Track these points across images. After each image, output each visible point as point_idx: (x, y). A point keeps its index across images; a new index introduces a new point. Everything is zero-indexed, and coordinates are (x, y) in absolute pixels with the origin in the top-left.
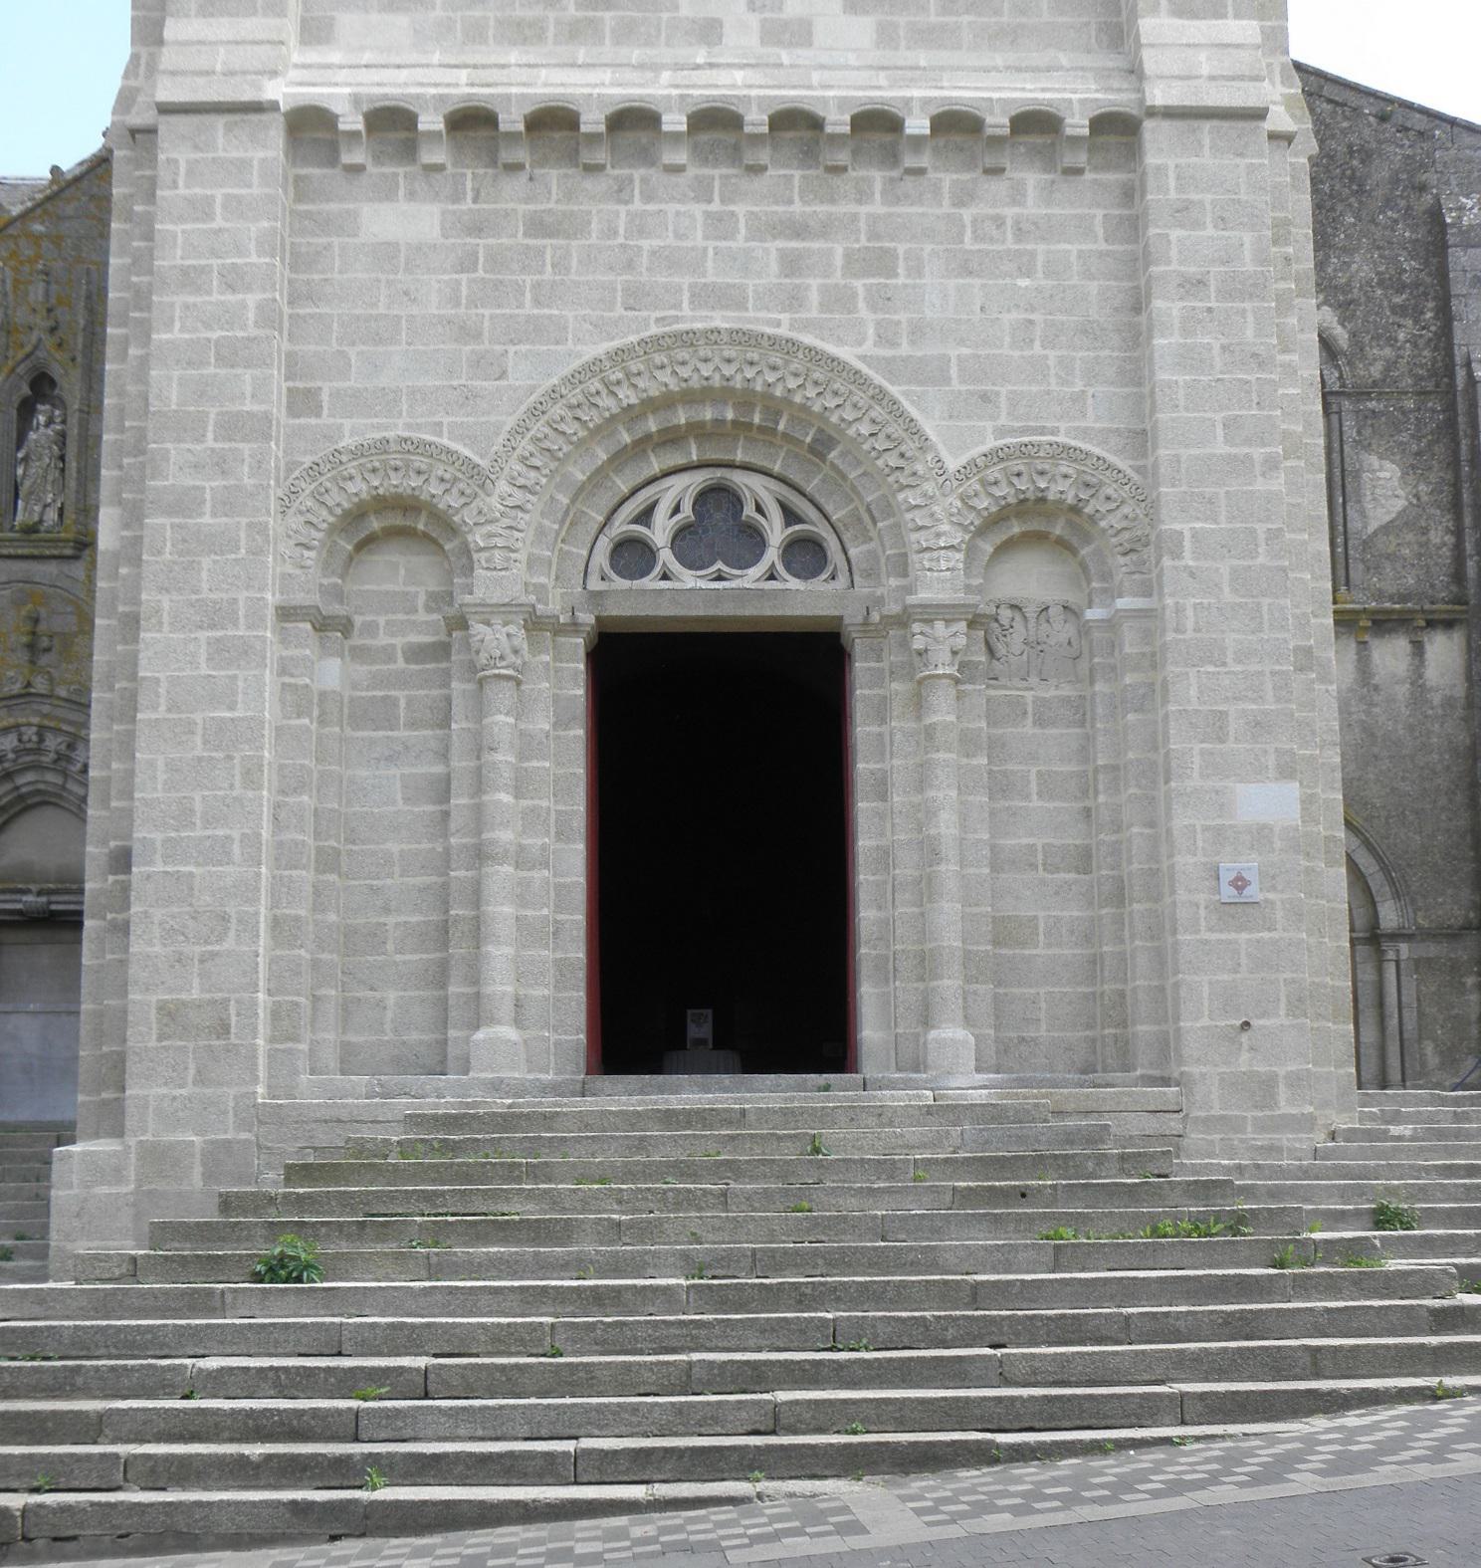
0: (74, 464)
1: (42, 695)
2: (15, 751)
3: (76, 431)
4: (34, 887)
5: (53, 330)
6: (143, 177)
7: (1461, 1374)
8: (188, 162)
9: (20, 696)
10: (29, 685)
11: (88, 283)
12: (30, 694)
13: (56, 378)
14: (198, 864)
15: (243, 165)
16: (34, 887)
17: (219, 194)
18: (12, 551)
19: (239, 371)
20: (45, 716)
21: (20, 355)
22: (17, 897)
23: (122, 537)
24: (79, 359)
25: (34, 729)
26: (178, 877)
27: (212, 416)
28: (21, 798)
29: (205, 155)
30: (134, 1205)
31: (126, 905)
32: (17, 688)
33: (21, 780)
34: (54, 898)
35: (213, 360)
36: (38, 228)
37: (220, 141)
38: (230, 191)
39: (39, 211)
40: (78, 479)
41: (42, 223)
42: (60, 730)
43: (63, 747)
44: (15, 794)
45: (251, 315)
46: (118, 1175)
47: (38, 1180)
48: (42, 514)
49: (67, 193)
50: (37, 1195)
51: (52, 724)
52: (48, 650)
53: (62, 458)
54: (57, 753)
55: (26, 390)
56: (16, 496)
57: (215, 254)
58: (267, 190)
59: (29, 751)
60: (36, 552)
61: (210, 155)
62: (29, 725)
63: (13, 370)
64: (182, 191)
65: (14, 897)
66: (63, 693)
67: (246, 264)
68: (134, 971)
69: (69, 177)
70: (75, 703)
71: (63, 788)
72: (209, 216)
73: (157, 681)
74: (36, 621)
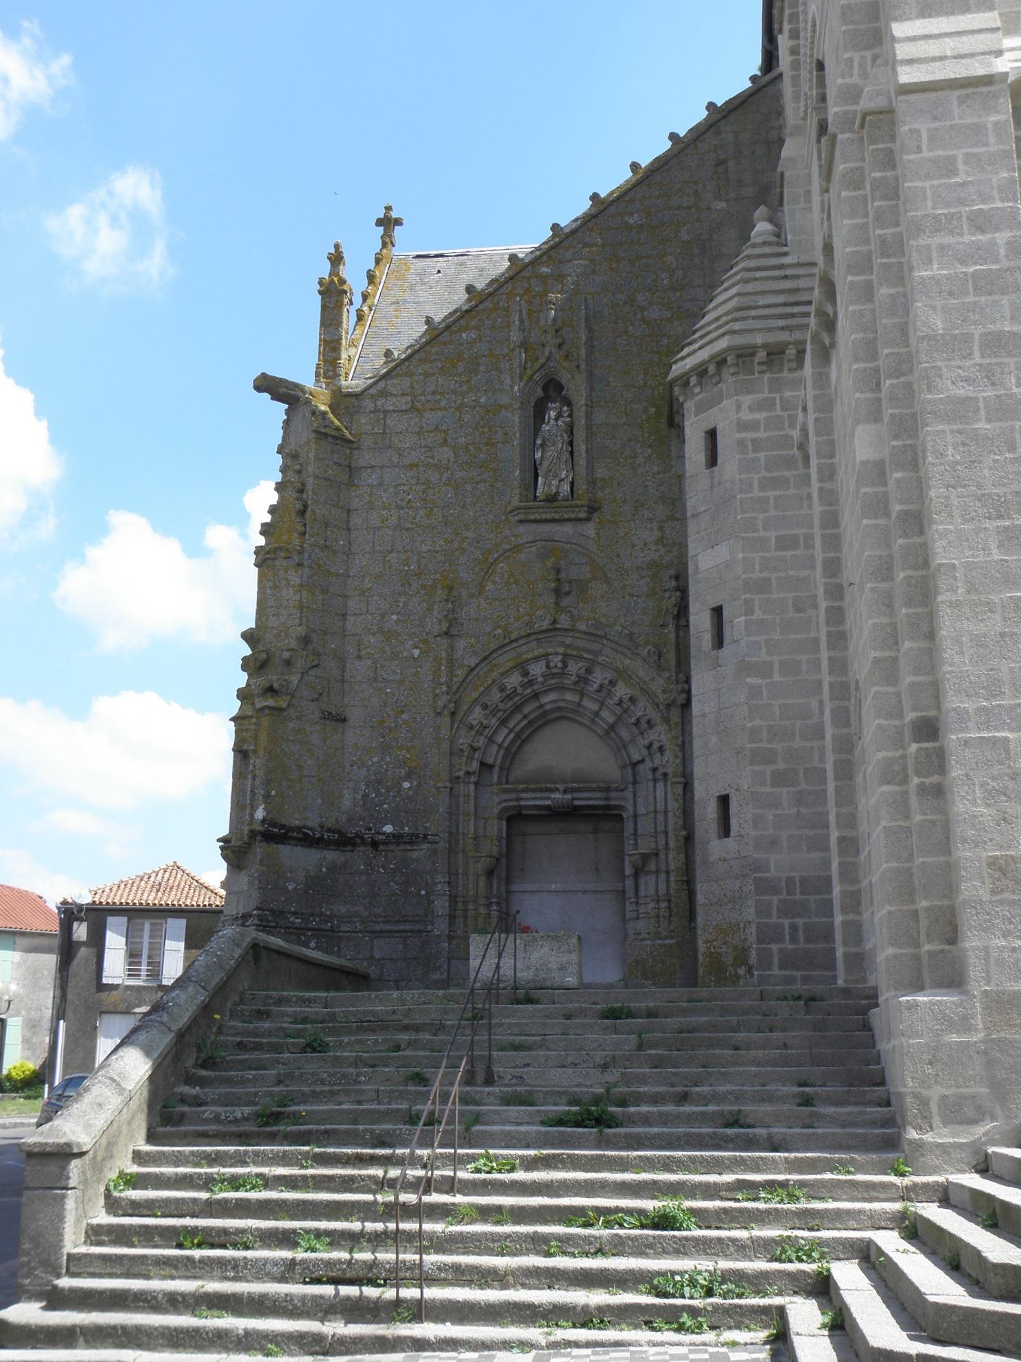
0: (583, 447)
1: (566, 630)
2: (543, 676)
3: (583, 421)
4: (561, 787)
5: (560, 346)
6: (877, 149)
7: (241, 1218)
8: (928, 130)
9: (547, 631)
10: (555, 621)
11: (586, 308)
12: (555, 629)
13: (564, 382)
14: (1011, 730)
15: (979, 129)
16: (561, 787)
17: (960, 154)
18: (537, 517)
19: (997, 297)
20: (567, 646)
21: (537, 366)
22: (547, 795)
23: (894, 447)
24: (583, 366)
25: (560, 657)
26: (995, 742)
27: (977, 337)
28: (545, 713)
29: (942, 124)
30: (985, 1052)
31: (942, 769)
32: (545, 624)
33: (545, 699)
34: (577, 795)
35: (971, 290)
36: (545, 270)
37: (956, 111)
38: (970, 150)
39: (545, 258)
40: (587, 458)
41: (547, 267)
42: (581, 657)
43: (583, 671)
44: (541, 711)
45: (1002, 251)
46: (964, 1024)
47: (771, 1031)
48: (558, 487)
49: (566, 243)
50: (785, 1044)
51: (575, 653)
52: (568, 593)
53: (571, 443)
54: (578, 676)
55: (540, 393)
56: (536, 476)
57: (961, 202)
58: (1002, 147)
59: (553, 675)
60: (557, 517)
61: (948, 123)
62: (557, 654)
63: (531, 378)
64: (926, 154)
65: (543, 795)
66: (583, 628)
67: (992, 209)
68: (958, 830)
69: (567, 230)
70: (593, 635)
71: (579, 704)
72: (953, 172)
73: (953, 567)
74: (558, 571)
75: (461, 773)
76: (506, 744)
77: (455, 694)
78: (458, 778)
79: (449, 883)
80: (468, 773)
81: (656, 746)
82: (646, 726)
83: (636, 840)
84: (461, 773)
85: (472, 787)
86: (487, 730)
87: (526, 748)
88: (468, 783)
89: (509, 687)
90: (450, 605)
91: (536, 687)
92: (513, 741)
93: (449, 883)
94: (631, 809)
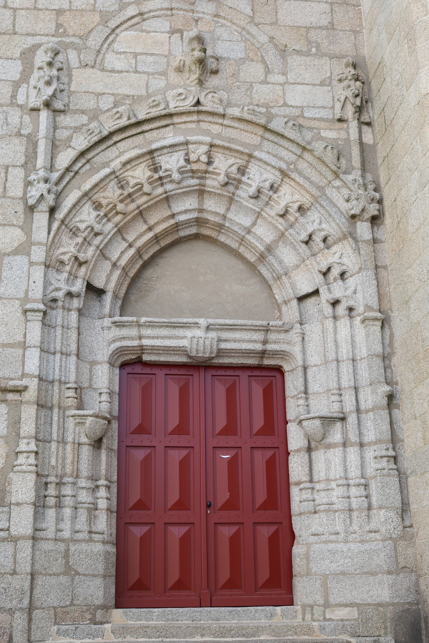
10: (198, 103)
43: (234, 169)
62: (201, 143)
75: (60, 294)
76: (123, 262)
77: (57, 183)
78: (55, 300)
79: (37, 453)
80: (70, 295)
81: (335, 272)
82: (322, 245)
83: (307, 399)
84: (60, 294)
85: (74, 315)
86: (99, 238)
87: (149, 273)
88: (69, 310)
89: (132, 182)
90: (54, 72)
91: (169, 187)
92: (132, 260)
93: (37, 453)
94: (299, 357)
